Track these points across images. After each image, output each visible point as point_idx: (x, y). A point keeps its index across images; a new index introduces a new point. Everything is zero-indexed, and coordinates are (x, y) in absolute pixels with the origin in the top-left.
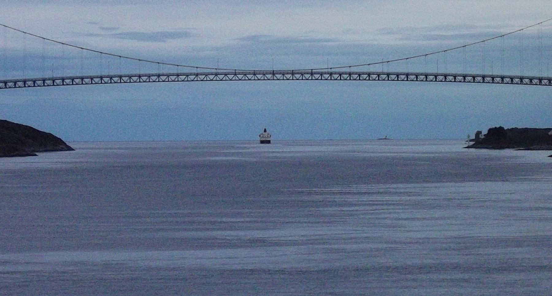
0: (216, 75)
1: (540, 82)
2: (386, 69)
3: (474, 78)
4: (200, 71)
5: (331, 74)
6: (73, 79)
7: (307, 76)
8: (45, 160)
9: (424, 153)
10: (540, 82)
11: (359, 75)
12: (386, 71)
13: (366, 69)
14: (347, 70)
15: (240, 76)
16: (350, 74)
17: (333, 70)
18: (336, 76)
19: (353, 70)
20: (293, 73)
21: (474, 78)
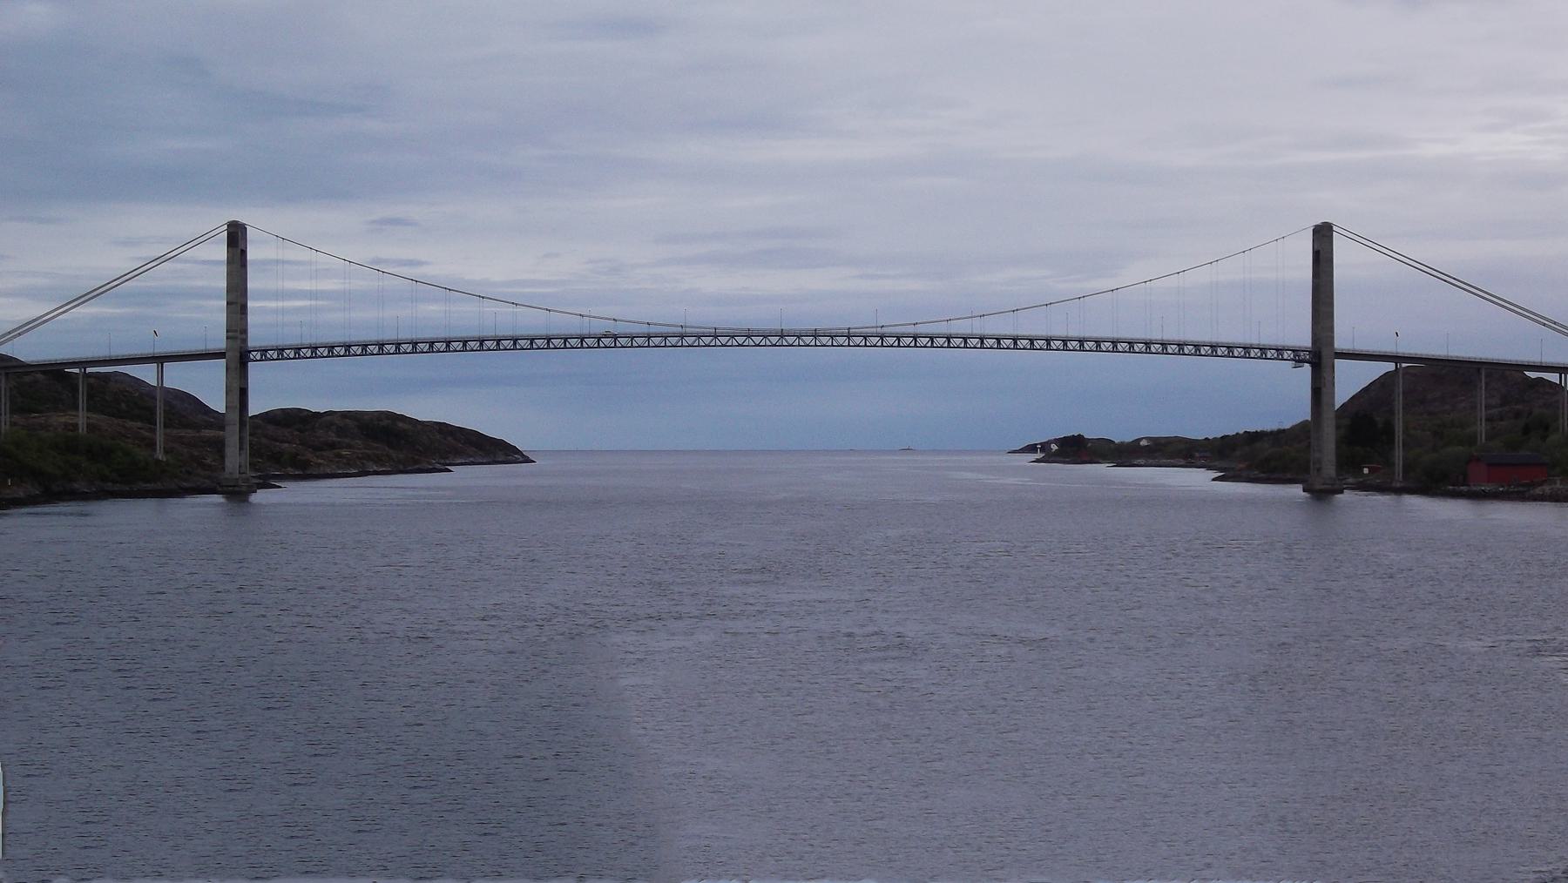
0: (682, 337)
1: (1082, 345)
2: (978, 327)
3: (465, 342)
4: (653, 330)
5: (882, 337)
6: (365, 346)
7: (841, 340)
8: (467, 478)
9: (59, 514)
10: (1082, 345)
11: (898, 338)
12: (977, 331)
13: (943, 329)
14: (911, 330)
15: (791, 340)
16: (915, 338)
17: (885, 330)
18: (891, 340)
19: (921, 329)
20: (816, 335)
21: (1032, 341)
